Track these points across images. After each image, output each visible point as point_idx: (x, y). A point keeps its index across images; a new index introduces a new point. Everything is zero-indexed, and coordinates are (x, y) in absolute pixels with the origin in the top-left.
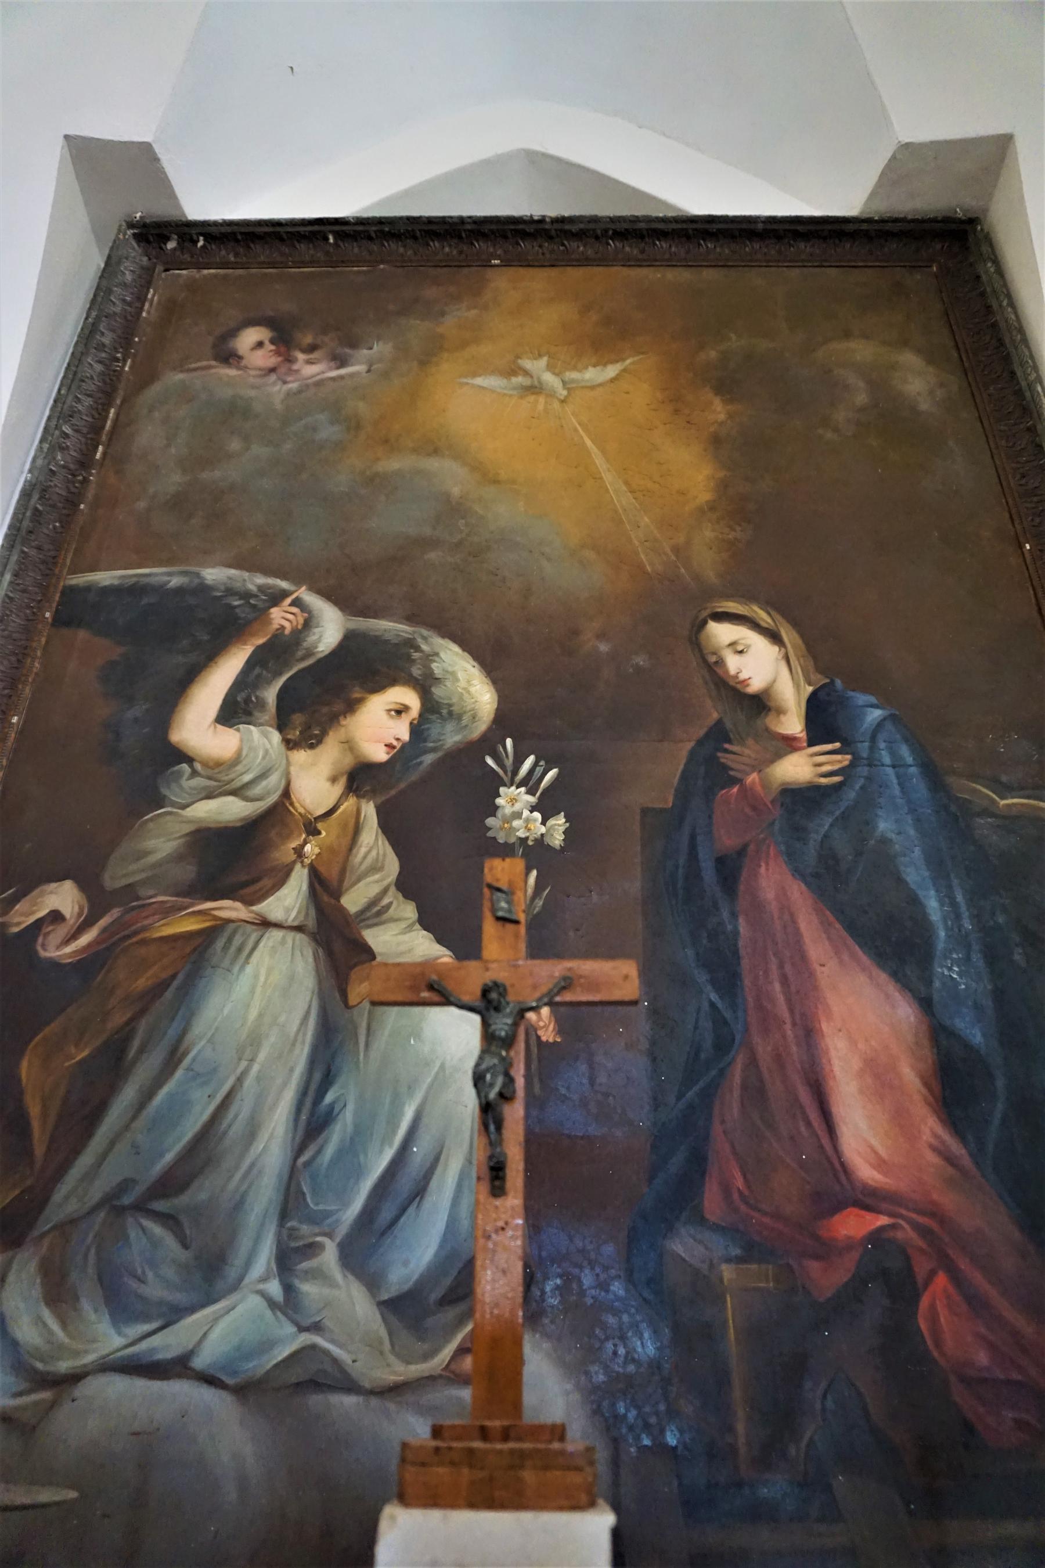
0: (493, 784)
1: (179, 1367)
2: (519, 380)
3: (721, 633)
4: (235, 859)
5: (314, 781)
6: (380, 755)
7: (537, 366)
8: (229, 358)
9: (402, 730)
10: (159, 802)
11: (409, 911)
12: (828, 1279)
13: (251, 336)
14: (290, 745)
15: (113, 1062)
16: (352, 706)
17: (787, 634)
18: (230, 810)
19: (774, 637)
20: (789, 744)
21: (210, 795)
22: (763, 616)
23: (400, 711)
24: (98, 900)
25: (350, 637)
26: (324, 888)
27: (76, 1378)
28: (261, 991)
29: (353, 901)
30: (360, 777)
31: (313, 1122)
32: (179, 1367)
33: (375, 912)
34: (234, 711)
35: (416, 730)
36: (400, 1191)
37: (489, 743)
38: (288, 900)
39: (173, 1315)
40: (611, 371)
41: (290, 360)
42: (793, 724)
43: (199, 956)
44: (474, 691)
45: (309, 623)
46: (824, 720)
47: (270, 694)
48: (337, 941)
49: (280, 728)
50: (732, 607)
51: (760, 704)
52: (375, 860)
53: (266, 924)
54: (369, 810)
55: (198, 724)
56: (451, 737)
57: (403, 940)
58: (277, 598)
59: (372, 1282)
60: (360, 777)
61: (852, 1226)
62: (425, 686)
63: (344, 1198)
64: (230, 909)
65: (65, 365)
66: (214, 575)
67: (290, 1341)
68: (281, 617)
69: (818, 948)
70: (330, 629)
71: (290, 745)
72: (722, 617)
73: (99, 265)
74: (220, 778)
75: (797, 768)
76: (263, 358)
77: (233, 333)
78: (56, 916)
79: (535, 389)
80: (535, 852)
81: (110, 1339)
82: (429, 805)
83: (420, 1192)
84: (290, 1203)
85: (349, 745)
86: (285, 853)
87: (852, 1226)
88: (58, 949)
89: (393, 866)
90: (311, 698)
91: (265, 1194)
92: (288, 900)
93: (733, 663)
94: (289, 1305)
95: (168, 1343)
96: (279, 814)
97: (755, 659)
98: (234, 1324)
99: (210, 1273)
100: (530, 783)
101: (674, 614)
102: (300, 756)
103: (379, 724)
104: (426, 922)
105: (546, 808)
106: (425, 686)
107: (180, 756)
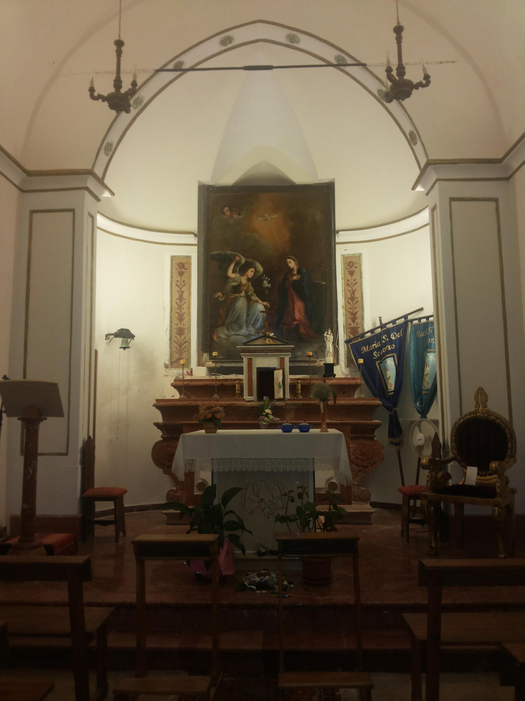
0: (263, 280)
1: (239, 335)
2: (264, 218)
3: (289, 260)
4: (237, 289)
5: (244, 280)
6: (251, 277)
7: (266, 215)
8: (223, 213)
9: (253, 274)
10: (227, 283)
11: (255, 295)
12: (293, 327)
13: (226, 209)
14: (241, 276)
15: (228, 311)
16: (247, 271)
17: (296, 261)
18: (235, 284)
19: (294, 261)
20: (295, 275)
21: (233, 282)
22: (293, 258)
23: (252, 271)
24: (224, 294)
25: (246, 262)
26: (246, 292)
27: (230, 336)
28: (241, 303)
29: (249, 294)
30: (249, 280)
31: (248, 315)
32: (239, 335)
33: (252, 295)
34: (234, 272)
35: (254, 274)
36: (256, 320)
37: (262, 275)
38: (243, 294)
39: (238, 331)
40: (277, 216)
41: (232, 214)
42: (295, 272)
43: (235, 300)
44: (261, 268)
45: (241, 259)
46: (299, 271)
47: (238, 269)
48: (248, 298)
49: (239, 273)
50: (290, 256)
51: (292, 270)
52: (251, 290)
53: (241, 296)
54: (250, 284)
55: (230, 273)
56: (258, 275)
57: (255, 298)
58: (236, 255)
59: (254, 328)
60: (249, 280)
61: (295, 323)
62: (255, 268)
63: (251, 321)
64: (237, 295)
65: (142, 512)
66: (228, 252)
67: (248, 333)
68: (237, 258)
69: (295, 298)
70: (243, 261)
71: (241, 276)
72: (289, 258)
73: (338, 237)
74: (234, 280)
75: (295, 278)
76: (228, 213)
77: (223, 208)
78: (219, 296)
79: (266, 220)
80: (268, 288)
81: (233, 333)
82: (256, 282)
83: (258, 320)
84: (247, 322)
85: (247, 276)
86: (242, 288)
87: (295, 323)
88: (221, 299)
89: (253, 290)
90: (242, 269)
91: (244, 321)
92: (243, 294)
93: (290, 264)
94: (248, 330)
95: (238, 333)
96: (240, 284)
97: (292, 264)
98: (244, 331)
99: (241, 328)
100: (267, 280)
101: (283, 258)
102: (242, 277)
103: (250, 273)
104: (257, 296)
105: (269, 283)
106: (255, 268)
107: (228, 277)
